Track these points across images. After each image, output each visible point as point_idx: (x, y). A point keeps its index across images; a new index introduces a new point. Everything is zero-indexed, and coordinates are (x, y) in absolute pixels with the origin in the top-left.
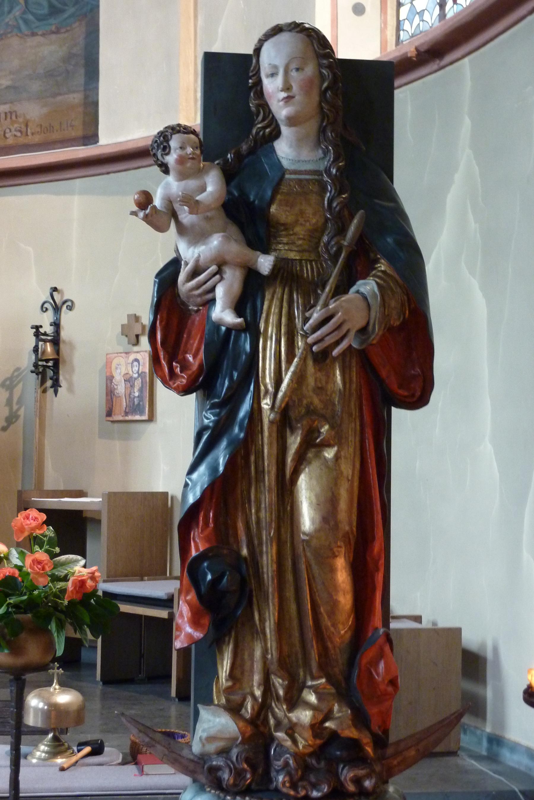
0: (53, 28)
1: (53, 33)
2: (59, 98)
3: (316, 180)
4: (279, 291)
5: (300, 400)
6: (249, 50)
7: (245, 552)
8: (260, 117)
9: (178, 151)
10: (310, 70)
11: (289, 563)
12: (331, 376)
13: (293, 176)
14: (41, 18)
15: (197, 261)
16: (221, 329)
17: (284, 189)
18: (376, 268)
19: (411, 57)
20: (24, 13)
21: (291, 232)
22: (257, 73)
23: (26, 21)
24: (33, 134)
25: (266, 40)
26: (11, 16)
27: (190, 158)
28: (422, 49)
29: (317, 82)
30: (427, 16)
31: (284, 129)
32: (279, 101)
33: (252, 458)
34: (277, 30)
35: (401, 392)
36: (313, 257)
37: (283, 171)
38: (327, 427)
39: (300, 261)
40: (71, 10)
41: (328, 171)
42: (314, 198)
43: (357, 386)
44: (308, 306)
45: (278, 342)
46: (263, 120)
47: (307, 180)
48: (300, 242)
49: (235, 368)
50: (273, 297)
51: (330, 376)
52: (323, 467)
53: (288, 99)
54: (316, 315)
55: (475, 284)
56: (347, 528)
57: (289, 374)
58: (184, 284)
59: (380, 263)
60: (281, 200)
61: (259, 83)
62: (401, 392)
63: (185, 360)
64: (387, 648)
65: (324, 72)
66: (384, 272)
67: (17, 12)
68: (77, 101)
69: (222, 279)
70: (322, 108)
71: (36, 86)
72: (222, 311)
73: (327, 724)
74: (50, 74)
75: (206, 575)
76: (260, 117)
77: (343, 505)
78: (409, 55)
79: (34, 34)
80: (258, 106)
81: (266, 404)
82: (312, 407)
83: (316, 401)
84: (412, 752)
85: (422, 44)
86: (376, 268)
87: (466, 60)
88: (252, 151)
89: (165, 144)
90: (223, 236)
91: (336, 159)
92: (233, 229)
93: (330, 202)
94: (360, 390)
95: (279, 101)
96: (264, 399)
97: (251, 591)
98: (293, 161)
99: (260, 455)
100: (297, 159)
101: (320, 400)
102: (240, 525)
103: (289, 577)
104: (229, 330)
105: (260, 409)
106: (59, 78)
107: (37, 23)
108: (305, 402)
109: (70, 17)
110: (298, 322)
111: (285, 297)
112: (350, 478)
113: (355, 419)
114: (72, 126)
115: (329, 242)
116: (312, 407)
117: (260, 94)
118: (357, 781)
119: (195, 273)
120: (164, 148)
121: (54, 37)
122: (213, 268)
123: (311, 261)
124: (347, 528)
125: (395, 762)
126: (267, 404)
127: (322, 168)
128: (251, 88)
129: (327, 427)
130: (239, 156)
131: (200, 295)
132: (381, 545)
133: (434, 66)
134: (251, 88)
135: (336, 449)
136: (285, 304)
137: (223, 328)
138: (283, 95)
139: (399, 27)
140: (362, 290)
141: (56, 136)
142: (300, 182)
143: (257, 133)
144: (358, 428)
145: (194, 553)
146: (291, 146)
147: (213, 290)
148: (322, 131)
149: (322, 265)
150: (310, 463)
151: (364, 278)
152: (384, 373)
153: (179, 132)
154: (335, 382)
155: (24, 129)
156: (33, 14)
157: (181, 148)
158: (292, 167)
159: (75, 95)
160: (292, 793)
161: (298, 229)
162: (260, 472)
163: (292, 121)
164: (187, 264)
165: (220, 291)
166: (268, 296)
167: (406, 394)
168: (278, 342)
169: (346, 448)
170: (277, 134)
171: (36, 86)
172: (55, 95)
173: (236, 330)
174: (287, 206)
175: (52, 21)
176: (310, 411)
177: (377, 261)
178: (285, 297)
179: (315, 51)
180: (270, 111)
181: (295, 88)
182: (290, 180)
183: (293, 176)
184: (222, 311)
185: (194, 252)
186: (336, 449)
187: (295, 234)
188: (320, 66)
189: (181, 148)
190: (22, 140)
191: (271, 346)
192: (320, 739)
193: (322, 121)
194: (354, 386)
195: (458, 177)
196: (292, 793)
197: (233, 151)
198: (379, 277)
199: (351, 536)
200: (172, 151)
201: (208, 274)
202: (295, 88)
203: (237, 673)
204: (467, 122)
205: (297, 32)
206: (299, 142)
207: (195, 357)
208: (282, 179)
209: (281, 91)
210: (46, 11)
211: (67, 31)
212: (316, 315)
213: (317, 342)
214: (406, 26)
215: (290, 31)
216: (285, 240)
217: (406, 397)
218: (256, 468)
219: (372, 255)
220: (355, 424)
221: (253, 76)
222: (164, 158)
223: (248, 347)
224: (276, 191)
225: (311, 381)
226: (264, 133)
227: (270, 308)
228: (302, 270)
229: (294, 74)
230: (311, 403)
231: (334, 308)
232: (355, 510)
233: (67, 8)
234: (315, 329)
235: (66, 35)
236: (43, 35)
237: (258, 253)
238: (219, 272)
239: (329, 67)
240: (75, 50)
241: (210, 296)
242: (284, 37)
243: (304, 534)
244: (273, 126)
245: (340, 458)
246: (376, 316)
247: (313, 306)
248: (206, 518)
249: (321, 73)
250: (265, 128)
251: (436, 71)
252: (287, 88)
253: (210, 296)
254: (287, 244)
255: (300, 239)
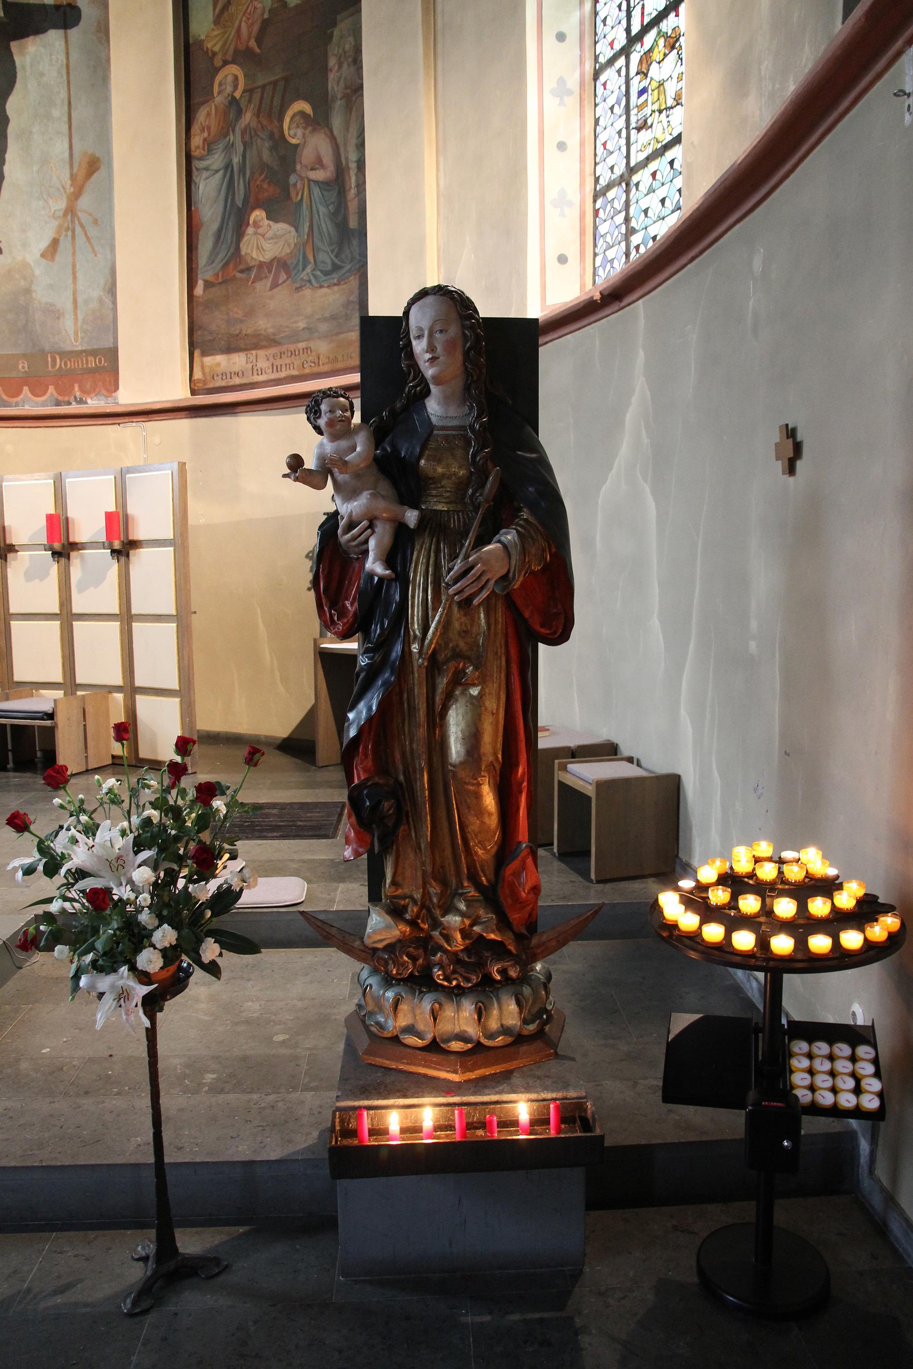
0: (335, 281)
1: (335, 285)
2: (342, 336)
3: (462, 435)
4: (427, 541)
5: (446, 644)
6: (400, 314)
7: (401, 778)
8: (411, 377)
9: (327, 414)
10: (454, 330)
11: (440, 788)
12: (476, 619)
13: (441, 432)
14: (326, 273)
15: (350, 515)
16: (374, 579)
17: (432, 445)
18: (519, 517)
19: (596, 300)
20: (314, 270)
21: (439, 485)
22: (406, 335)
23: (315, 277)
24: (323, 364)
25: (414, 304)
26: (305, 273)
27: (340, 421)
28: (606, 293)
29: (460, 342)
30: (616, 264)
31: (432, 387)
32: (425, 362)
33: (405, 696)
34: (423, 294)
35: (543, 630)
36: (459, 507)
37: (431, 427)
38: (471, 668)
39: (448, 511)
40: (348, 267)
41: (472, 427)
42: (459, 453)
43: (502, 626)
44: (453, 557)
45: (425, 591)
46: (414, 380)
47: (453, 435)
48: (448, 494)
49: (385, 615)
50: (422, 547)
51: (474, 620)
52: (468, 704)
53: (433, 360)
54: (458, 565)
55: (648, 490)
56: (491, 759)
57: (434, 623)
58: (342, 536)
59: (523, 511)
60: (429, 455)
61: (409, 344)
62: (543, 630)
63: (344, 606)
64: (529, 861)
65: (467, 332)
66: (526, 520)
67: (309, 269)
68: (354, 338)
69: (373, 532)
70: (466, 368)
71: (324, 327)
72: (374, 563)
73: (475, 928)
74: (333, 318)
75: (365, 802)
76: (411, 377)
77: (487, 738)
78: (595, 298)
79: (321, 287)
80: (409, 366)
81: (415, 648)
82: (458, 650)
83: (462, 644)
84: (554, 943)
85: (605, 289)
86: (519, 517)
87: (640, 302)
88: (405, 409)
89: (316, 408)
90: (371, 494)
91: (479, 416)
92: (385, 487)
93: (474, 456)
94: (506, 628)
95: (425, 362)
96: (413, 643)
97: (407, 813)
98: (442, 418)
99: (411, 691)
100: (445, 415)
101: (465, 643)
102: (398, 755)
103: (442, 799)
104: (381, 579)
105: (410, 652)
106: (341, 321)
107: (324, 278)
108: (451, 645)
109: (348, 271)
110: (444, 571)
111: (433, 547)
112: (494, 712)
113: (500, 657)
114: (351, 357)
115: (473, 494)
116: (458, 650)
117: (411, 355)
118: (503, 972)
119: (351, 526)
120: (315, 413)
121: (336, 288)
122: (365, 523)
123: (458, 512)
124: (491, 759)
125: (539, 951)
126: (415, 648)
127: (467, 423)
128: (402, 349)
129: (471, 668)
130: (393, 414)
131: (357, 546)
132: (524, 769)
133: (615, 306)
134: (402, 349)
135: (479, 688)
136: (432, 554)
137: (376, 579)
138: (428, 356)
139: (595, 274)
140: (503, 539)
141: (340, 365)
142: (446, 437)
143: (409, 391)
144: (504, 663)
145: (356, 781)
146: (439, 404)
147: (366, 542)
148: (467, 388)
149: (468, 515)
150: (457, 700)
151: (507, 528)
152: (527, 614)
153: (329, 396)
154: (479, 625)
155: (317, 361)
156: (320, 270)
157: (330, 411)
158: (440, 424)
159: (353, 334)
160: (446, 983)
161: (444, 482)
162: (412, 709)
163: (437, 380)
164: (342, 518)
165: (372, 543)
166: (417, 547)
167: (548, 632)
168: (425, 591)
169: (491, 685)
170: (427, 393)
171: (324, 327)
172: (338, 334)
173: (388, 580)
174: (434, 461)
175: (334, 275)
176: (457, 655)
177: (520, 510)
178: (433, 547)
179: (458, 312)
180: (420, 371)
181: (439, 349)
182: (438, 435)
183: (441, 432)
184: (374, 563)
185: (347, 508)
186: (479, 688)
187: (442, 487)
188: (463, 327)
189: (330, 411)
190: (316, 370)
191: (419, 595)
192: (470, 940)
193: (467, 380)
194: (500, 626)
195: (635, 399)
196: (446, 983)
197: (388, 409)
198: (521, 526)
199: (496, 765)
200: (323, 415)
201: (360, 528)
202: (439, 349)
203: (399, 879)
204: (641, 353)
205: (441, 295)
206: (446, 400)
207: (352, 604)
208: (430, 434)
209: (427, 352)
210: (329, 267)
211: (345, 283)
212: (458, 565)
213: (458, 593)
214: (600, 272)
215: (435, 294)
216: (434, 492)
217: (547, 634)
218: (409, 705)
219: (516, 504)
220: (501, 661)
221: (404, 337)
222: (316, 422)
223: (397, 598)
224: (424, 448)
225: (456, 625)
226: (415, 391)
227: (418, 558)
228: (449, 520)
229: (438, 335)
230: (457, 646)
231: (474, 559)
232: (500, 739)
233: (343, 265)
234: (456, 580)
235: (345, 286)
236: (328, 287)
237: (406, 507)
238: (371, 526)
239: (472, 328)
240: (351, 299)
241: (364, 547)
242: (429, 300)
243: (451, 765)
244: (423, 385)
245: (484, 695)
246: (516, 564)
247: (457, 557)
248: (366, 748)
249: (464, 334)
250: (415, 387)
251: (617, 312)
252: (431, 348)
253: (364, 547)
254: (436, 496)
255: (448, 491)
